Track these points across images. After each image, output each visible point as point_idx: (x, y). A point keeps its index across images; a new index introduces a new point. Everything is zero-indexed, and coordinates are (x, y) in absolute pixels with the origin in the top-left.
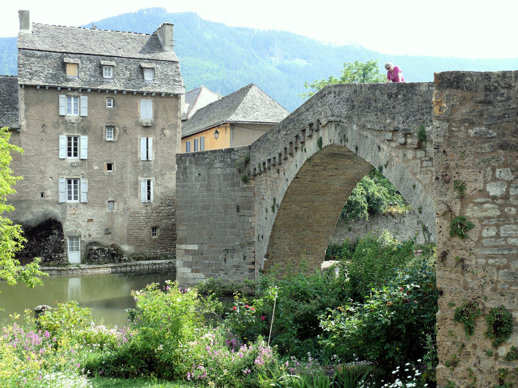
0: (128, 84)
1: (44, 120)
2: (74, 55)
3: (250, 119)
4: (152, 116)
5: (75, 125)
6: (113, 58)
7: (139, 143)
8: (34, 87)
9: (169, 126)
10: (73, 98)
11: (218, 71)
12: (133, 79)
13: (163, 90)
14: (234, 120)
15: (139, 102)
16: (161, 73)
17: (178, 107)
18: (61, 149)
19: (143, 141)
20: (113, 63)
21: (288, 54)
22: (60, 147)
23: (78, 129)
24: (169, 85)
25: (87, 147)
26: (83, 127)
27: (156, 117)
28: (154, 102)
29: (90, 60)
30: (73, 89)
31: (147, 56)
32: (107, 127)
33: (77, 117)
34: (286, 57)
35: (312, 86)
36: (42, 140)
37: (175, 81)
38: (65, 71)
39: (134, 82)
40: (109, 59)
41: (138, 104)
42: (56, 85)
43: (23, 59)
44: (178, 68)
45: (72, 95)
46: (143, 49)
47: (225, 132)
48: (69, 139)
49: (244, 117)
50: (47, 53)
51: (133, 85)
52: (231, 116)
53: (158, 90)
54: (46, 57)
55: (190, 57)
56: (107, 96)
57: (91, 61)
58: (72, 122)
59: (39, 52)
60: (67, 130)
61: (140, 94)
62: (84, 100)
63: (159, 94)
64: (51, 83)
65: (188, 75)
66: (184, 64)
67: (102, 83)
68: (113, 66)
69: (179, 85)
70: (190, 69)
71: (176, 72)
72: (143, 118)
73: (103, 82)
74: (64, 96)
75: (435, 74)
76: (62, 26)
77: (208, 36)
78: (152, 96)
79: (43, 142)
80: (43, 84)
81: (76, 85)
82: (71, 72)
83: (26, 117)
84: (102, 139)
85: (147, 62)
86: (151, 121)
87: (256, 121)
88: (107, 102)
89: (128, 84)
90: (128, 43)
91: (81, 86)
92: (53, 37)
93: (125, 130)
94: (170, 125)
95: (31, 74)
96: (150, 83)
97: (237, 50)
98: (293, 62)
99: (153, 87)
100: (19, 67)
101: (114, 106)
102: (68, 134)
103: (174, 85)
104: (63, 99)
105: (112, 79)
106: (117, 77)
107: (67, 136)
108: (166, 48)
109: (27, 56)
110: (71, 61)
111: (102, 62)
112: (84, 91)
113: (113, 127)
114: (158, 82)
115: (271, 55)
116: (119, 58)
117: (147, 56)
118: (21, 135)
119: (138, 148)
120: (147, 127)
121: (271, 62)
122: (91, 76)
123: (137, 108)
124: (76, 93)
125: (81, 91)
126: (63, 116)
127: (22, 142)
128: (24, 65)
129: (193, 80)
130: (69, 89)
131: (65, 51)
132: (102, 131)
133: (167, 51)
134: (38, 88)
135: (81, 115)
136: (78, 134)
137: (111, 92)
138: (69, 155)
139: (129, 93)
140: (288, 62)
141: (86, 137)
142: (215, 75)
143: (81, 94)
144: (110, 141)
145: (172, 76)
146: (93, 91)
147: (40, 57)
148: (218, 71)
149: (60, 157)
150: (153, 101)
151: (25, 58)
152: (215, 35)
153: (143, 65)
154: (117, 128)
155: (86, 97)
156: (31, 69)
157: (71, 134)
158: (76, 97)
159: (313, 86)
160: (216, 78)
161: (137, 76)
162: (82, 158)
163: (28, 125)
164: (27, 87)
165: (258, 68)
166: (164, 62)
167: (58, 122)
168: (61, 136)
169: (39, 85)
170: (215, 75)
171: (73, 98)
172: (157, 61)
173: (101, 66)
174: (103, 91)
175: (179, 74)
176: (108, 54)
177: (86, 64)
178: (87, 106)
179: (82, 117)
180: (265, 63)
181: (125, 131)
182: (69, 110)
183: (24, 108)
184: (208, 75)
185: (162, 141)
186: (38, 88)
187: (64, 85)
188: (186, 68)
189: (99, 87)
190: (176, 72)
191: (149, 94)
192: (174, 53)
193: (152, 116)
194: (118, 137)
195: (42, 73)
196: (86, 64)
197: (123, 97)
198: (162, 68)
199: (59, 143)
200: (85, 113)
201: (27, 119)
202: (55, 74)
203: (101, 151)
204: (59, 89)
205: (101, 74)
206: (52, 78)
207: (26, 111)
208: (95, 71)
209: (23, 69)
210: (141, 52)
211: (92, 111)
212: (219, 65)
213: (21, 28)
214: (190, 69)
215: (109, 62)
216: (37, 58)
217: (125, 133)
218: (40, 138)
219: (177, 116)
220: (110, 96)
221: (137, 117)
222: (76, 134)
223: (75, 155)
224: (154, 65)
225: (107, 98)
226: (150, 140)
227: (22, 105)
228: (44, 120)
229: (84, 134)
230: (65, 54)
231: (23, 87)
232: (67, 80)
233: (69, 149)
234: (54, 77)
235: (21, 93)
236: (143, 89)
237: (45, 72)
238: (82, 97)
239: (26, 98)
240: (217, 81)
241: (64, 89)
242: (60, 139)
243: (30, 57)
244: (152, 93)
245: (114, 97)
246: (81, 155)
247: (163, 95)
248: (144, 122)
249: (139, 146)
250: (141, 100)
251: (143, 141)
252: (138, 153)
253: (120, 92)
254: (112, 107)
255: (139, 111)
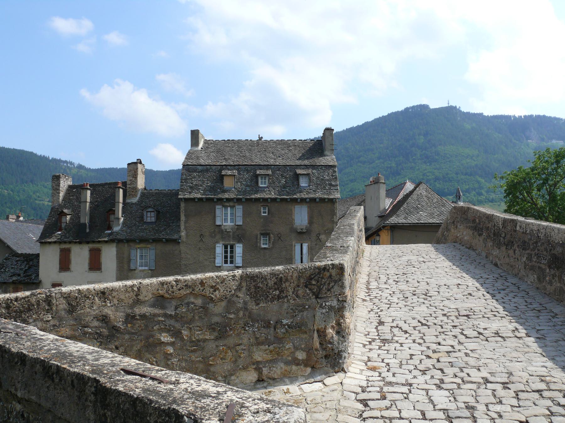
0: (283, 191)
1: (201, 230)
2: (232, 167)
3: (413, 219)
4: (307, 222)
5: (231, 234)
6: (269, 167)
7: (293, 248)
8: (193, 200)
9: (325, 231)
10: (229, 209)
11: (478, 156)
12: (288, 186)
13: (319, 195)
14: (393, 222)
15: (293, 208)
16: (318, 178)
17: (334, 211)
18: (217, 258)
19: (298, 247)
20: (270, 172)
21: (544, 137)
22: (216, 255)
23: (233, 237)
24: (325, 190)
25: (241, 255)
26: (238, 235)
27: (311, 222)
28: (309, 207)
29: (247, 170)
30: (228, 200)
31: (306, 162)
32: (262, 234)
33: (232, 225)
34: (543, 140)
35: (501, 178)
36: (200, 249)
37: (331, 185)
38: (222, 183)
39: (289, 189)
40: (265, 167)
41: (293, 211)
42: (213, 197)
43: (185, 175)
44: (335, 172)
45: (228, 205)
46: (303, 155)
47: (387, 234)
48: (226, 247)
49: (406, 218)
50: (208, 167)
51: (288, 192)
52: (392, 219)
53: (312, 196)
54: (207, 170)
55: (452, 146)
56: (262, 204)
57: (248, 172)
58: (228, 231)
59: (201, 167)
60: (223, 238)
61: (295, 201)
62: (239, 209)
63: (313, 200)
64: (209, 195)
65: (450, 162)
66: (446, 152)
67: (257, 192)
68: (268, 175)
69: (335, 189)
70: (451, 156)
71: (332, 176)
72: (298, 224)
73: (258, 191)
74: (220, 207)
75: (60, 272)
76: (249, 139)
77: (468, 126)
78: (306, 202)
79: (201, 251)
80: (201, 196)
81: (232, 196)
82: (228, 183)
83: (186, 228)
84: (257, 246)
85: (303, 169)
86: (306, 227)
87: (419, 222)
88: (262, 210)
89: (283, 191)
90: (290, 150)
91: (235, 197)
92: (218, 152)
93: (279, 237)
94: (326, 230)
95: (191, 187)
96: (305, 190)
97: (495, 136)
98: (549, 143)
99: (308, 193)
100: (182, 182)
101: (268, 214)
102: (223, 242)
103: (330, 189)
104: (219, 210)
105: (267, 187)
106: (273, 185)
107: (223, 244)
108: (326, 153)
109: (190, 172)
110: (229, 173)
111: (258, 172)
112: (239, 201)
113: (268, 234)
114: (314, 188)
115: (528, 138)
116: (276, 167)
117: (306, 162)
118: (181, 245)
119: (293, 254)
120: (301, 233)
121: (528, 145)
122: (247, 186)
123: (292, 214)
124: (231, 204)
125: (236, 201)
126: (220, 226)
127: (182, 252)
128: (186, 179)
129: (455, 166)
130: (225, 200)
131: (228, 164)
132: (257, 238)
133: (327, 156)
134: (196, 200)
135: (236, 224)
136: (234, 243)
137: (265, 200)
138: (226, 262)
139: (282, 200)
140: (545, 144)
141: (241, 245)
142: (474, 161)
143: (236, 204)
144: (265, 248)
145: (328, 180)
146: (247, 200)
147: (201, 171)
148: (478, 156)
149: (217, 265)
150: (308, 207)
151: (188, 174)
152: (474, 125)
153: (299, 171)
154: (271, 235)
155: (241, 207)
156: (192, 183)
157: (227, 243)
158: (232, 207)
159: (502, 178)
160: (475, 163)
161: (293, 183)
162: (237, 265)
163: (187, 235)
164: (187, 200)
165: (516, 151)
166: (321, 167)
167: (214, 231)
168: (217, 245)
169: (196, 198)
170: (474, 161)
171: (229, 209)
172: (313, 167)
173: (257, 176)
174: (257, 200)
175: (336, 178)
176: (266, 163)
177: (243, 175)
178: (242, 215)
179: (238, 225)
180: (523, 147)
181: (280, 238)
182: (226, 220)
183: (184, 219)
184: (468, 161)
185: (317, 246)
186: (196, 200)
187: (220, 196)
188: (448, 156)
189: (253, 197)
190: (332, 176)
191: (303, 201)
192: (334, 157)
193: (307, 222)
194: (273, 244)
195: (201, 186)
196: (243, 175)
197: (277, 205)
198: (318, 174)
199: (215, 252)
200: (240, 223)
201: (186, 230)
202: (214, 186)
203: (255, 259)
204: (215, 200)
205: (257, 183)
206: (210, 191)
207: (186, 222)
208: (251, 180)
209: (185, 183)
210: (299, 159)
211: (248, 220)
212: (479, 151)
213: (192, 146)
214: (451, 156)
215: (265, 171)
216: (199, 172)
217: (280, 240)
218: (198, 247)
219: (333, 221)
220: (265, 204)
221: (292, 222)
222: (232, 243)
223: (232, 262)
224: (310, 171)
225: (262, 206)
226: (305, 246)
227: (183, 218)
228: (201, 230)
229: (239, 242)
230: (224, 167)
231: (183, 200)
232: (224, 191)
233: (226, 257)
234: (212, 189)
235: (183, 205)
236: (297, 196)
237: (205, 185)
238: (237, 207)
239: (186, 211)
240: (476, 165)
241: (220, 200)
242: (216, 248)
243: (193, 172)
244: (306, 199)
245: (269, 205)
246: (236, 262)
247: (318, 200)
248: (298, 228)
249: (294, 252)
250: (296, 206)
251: (298, 247)
252: (293, 259)
253: (274, 200)
254: (266, 214)
255: (293, 217)
